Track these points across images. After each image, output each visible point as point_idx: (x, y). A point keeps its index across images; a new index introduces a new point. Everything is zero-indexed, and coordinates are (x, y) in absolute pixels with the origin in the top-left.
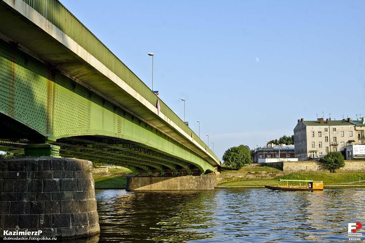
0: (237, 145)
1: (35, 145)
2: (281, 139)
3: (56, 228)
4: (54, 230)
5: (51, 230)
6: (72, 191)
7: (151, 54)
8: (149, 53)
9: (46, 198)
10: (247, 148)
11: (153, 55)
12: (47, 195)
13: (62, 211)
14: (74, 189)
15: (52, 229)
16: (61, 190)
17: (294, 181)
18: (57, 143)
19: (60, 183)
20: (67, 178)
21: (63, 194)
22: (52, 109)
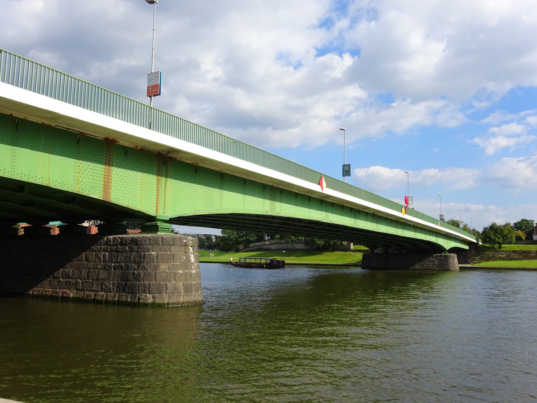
0: (519, 220)
1: (514, 264)
2: (485, 230)
3: (151, 295)
4: (149, 296)
5: (147, 296)
6: (168, 263)
7: (343, 128)
8: (341, 128)
9: (145, 268)
10: (487, 228)
11: (344, 130)
12: (146, 266)
13: (157, 280)
14: (169, 261)
15: (148, 295)
16: (157, 262)
17: (147, 235)
18: (170, 221)
19: (157, 256)
20: (164, 251)
21: (158, 265)
22: (163, 192)
